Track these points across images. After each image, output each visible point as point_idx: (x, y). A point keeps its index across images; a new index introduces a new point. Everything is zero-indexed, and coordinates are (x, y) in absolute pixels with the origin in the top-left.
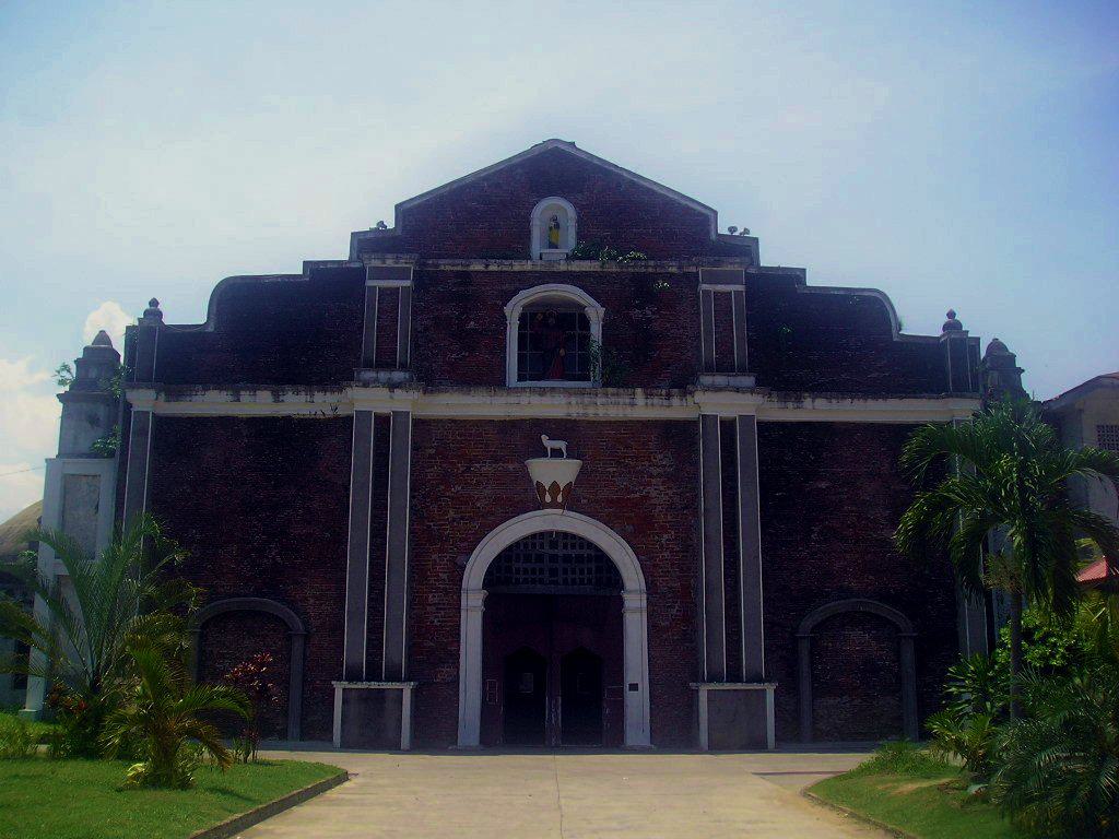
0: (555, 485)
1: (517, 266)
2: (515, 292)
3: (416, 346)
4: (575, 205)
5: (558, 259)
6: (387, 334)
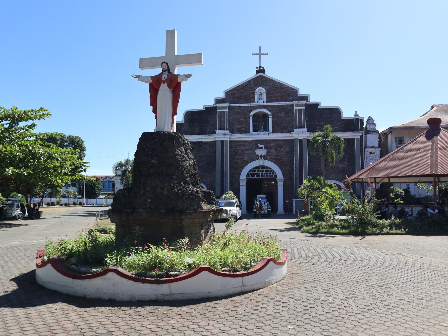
0: (261, 156)
1: (252, 104)
2: (252, 111)
3: (229, 124)
4: (265, 89)
5: (261, 103)
6: (222, 122)
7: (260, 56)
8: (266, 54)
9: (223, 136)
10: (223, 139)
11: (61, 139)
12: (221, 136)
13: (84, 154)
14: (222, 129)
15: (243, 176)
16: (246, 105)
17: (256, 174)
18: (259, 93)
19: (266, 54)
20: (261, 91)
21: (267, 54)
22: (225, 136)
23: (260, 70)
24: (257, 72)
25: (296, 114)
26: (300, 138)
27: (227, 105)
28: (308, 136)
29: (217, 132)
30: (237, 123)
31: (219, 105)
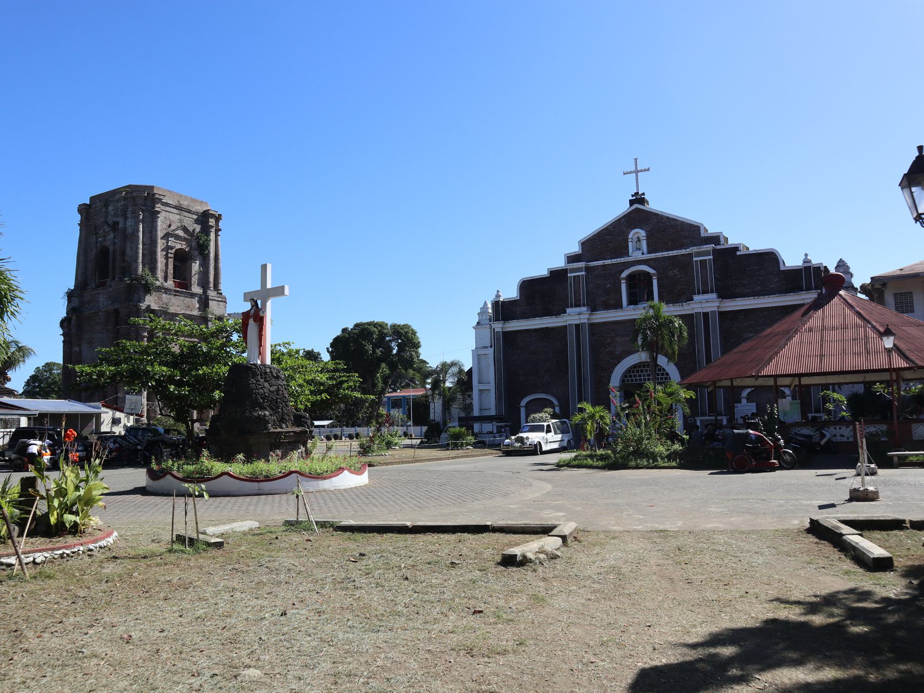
1: (623, 260)
5: (635, 255)
6: (577, 292)
7: (637, 175)
8: (645, 170)
9: (577, 317)
10: (578, 322)
11: (379, 331)
12: (575, 316)
13: (417, 352)
14: (577, 305)
15: (615, 381)
16: (614, 261)
17: (640, 376)
18: (635, 240)
19: (645, 170)
20: (638, 234)
21: (648, 170)
22: (581, 317)
23: (638, 199)
24: (632, 202)
25: (697, 269)
26: (705, 310)
27: (582, 264)
28: (718, 307)
29: (568, 310)
30: (601, 293)
31: (571, 266)
